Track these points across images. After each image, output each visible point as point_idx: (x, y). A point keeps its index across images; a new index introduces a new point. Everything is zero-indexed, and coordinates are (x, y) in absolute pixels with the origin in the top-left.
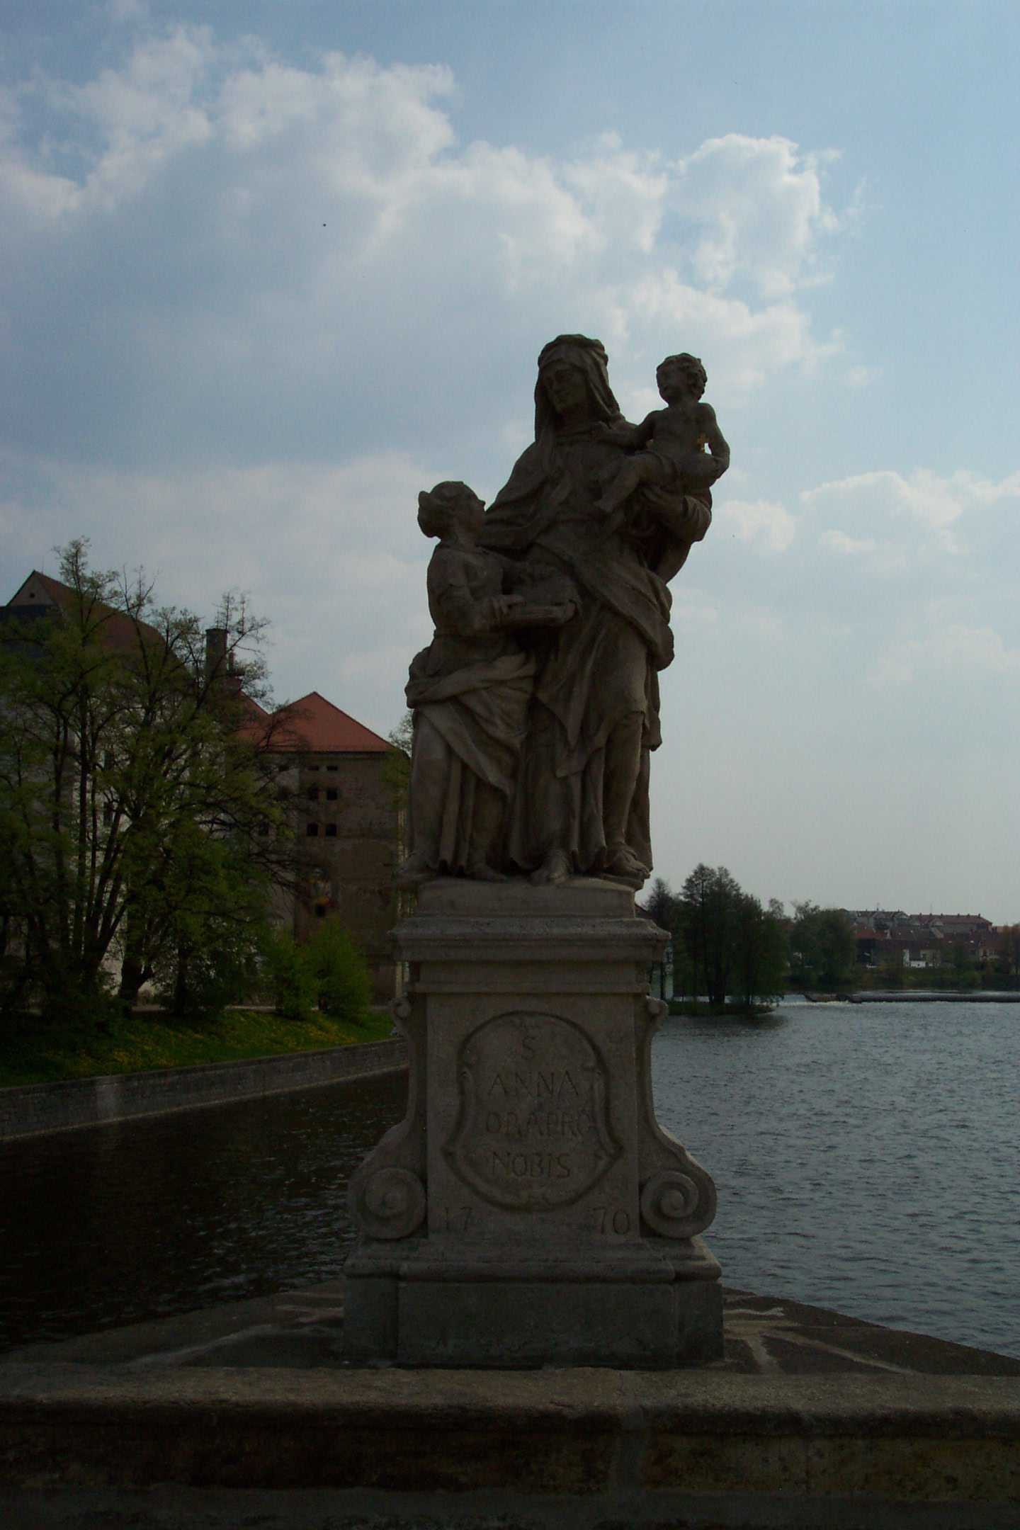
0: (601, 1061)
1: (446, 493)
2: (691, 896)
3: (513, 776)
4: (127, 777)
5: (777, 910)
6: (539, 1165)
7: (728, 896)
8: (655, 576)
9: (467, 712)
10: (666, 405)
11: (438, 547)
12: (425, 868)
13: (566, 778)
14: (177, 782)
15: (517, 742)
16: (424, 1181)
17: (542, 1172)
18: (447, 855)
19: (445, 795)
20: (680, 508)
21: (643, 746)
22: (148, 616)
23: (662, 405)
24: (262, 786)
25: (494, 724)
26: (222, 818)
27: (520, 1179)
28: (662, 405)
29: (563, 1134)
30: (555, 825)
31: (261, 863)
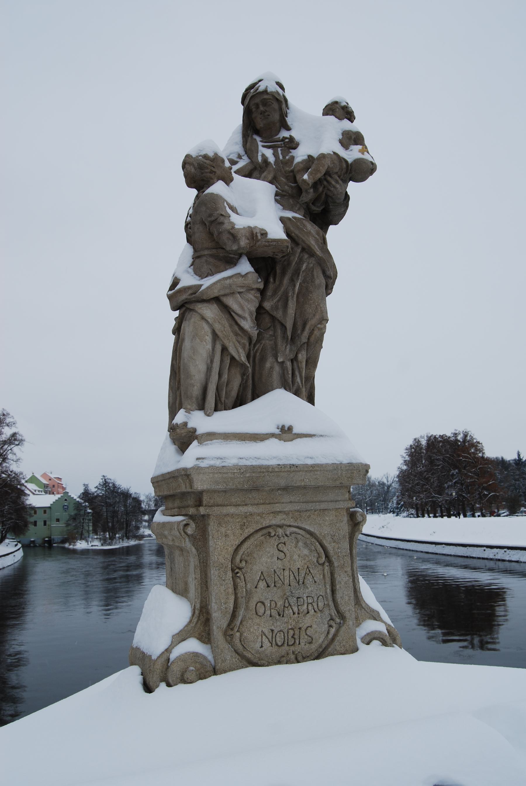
9: (226, 309)
13: (283, 363)
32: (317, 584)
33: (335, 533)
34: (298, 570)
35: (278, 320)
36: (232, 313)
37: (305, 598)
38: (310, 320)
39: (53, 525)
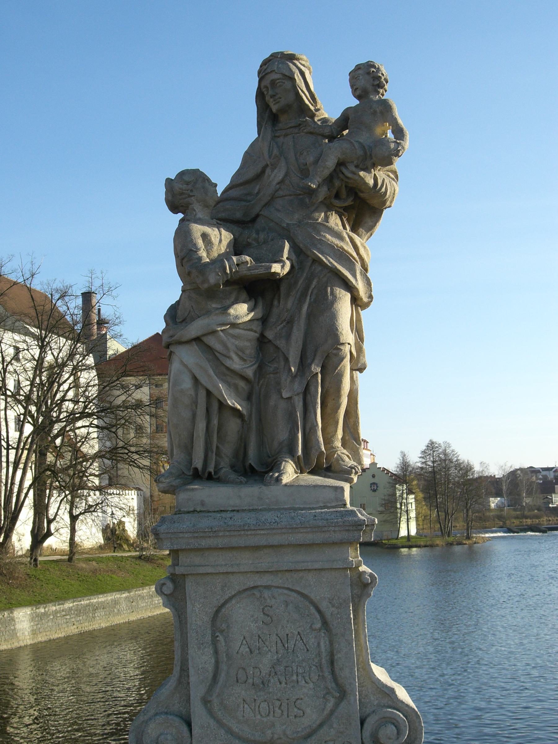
0: (325, 623)
1: (186, 178)
2: (425, 463)
3: (249, 398)
4: (28, 398)
5: (485, 470)
6: (280, 708)
7: (451, 461)
8: (356, 236)
9: (209, 350)
10: (357, 102)
11: (182, 221)
12: (181, 475)
13: (290, 398)
14: (63, 399)
15: (250, 373)
16: (189, 724)
17: (282, 714)
18: (198, 463)
19: (194, 416)
20: (371, 182)
21: (352, 370)
22: (37, 285)
23: (355, 102)
24: (124, 399)
25: (229, 358)
26: (96, 424)
27: (265, 720)
28: (355, 102)
29: (298, 682)
30: (282, 435)
31: (125, 453)
32: (310, 652)
33: (334, 596)
34: (287, 637)
35: (281, 351)
36: (217, 354)
37: (295, 668)
38: (322, 346)
39: (353, 565)
